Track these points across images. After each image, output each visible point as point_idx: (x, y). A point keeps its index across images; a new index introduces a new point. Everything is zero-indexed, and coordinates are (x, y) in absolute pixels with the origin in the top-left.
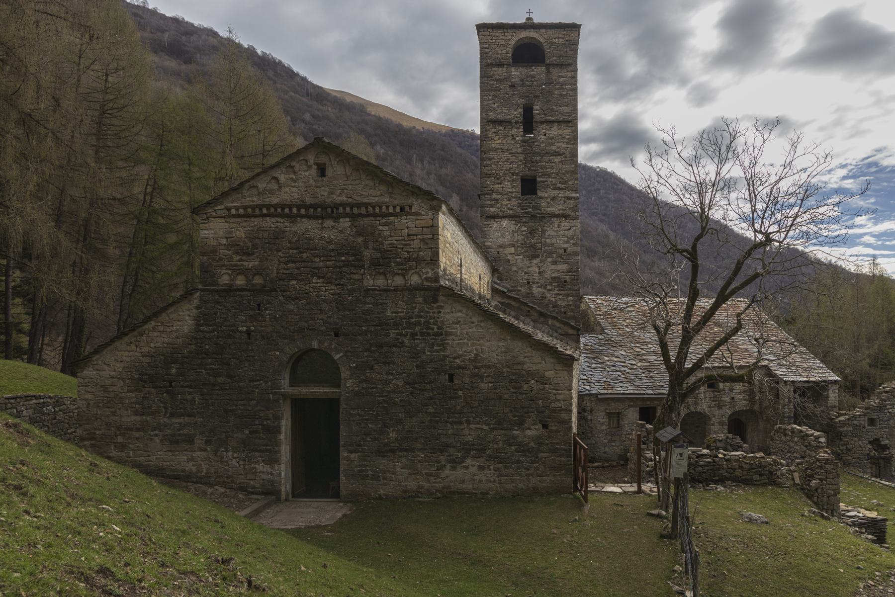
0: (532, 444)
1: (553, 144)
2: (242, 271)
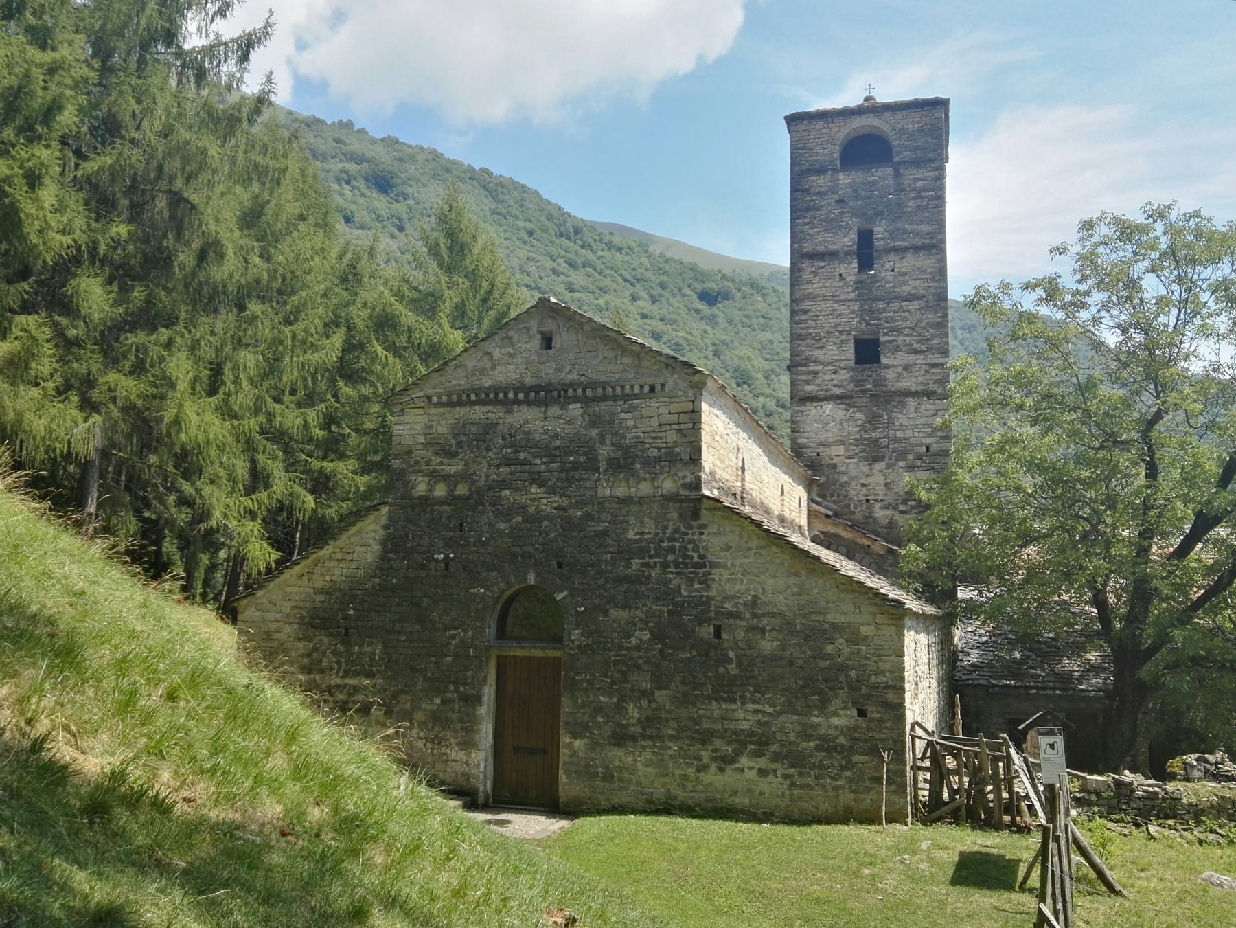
1: (905, 283)
2: (446, 478)
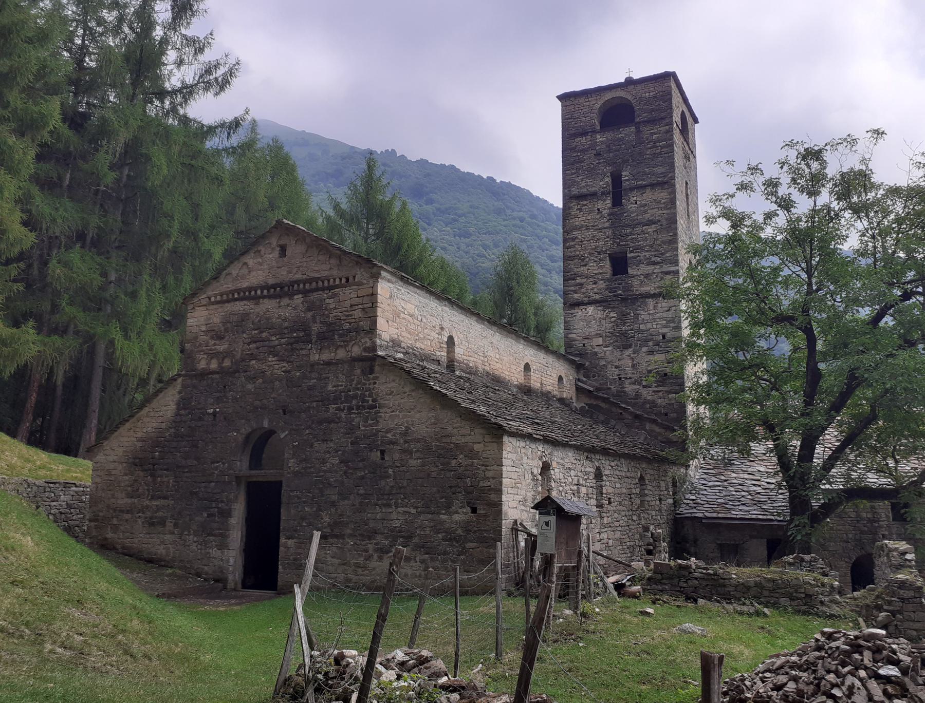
0: (460, 531)
1: (645, 212)
